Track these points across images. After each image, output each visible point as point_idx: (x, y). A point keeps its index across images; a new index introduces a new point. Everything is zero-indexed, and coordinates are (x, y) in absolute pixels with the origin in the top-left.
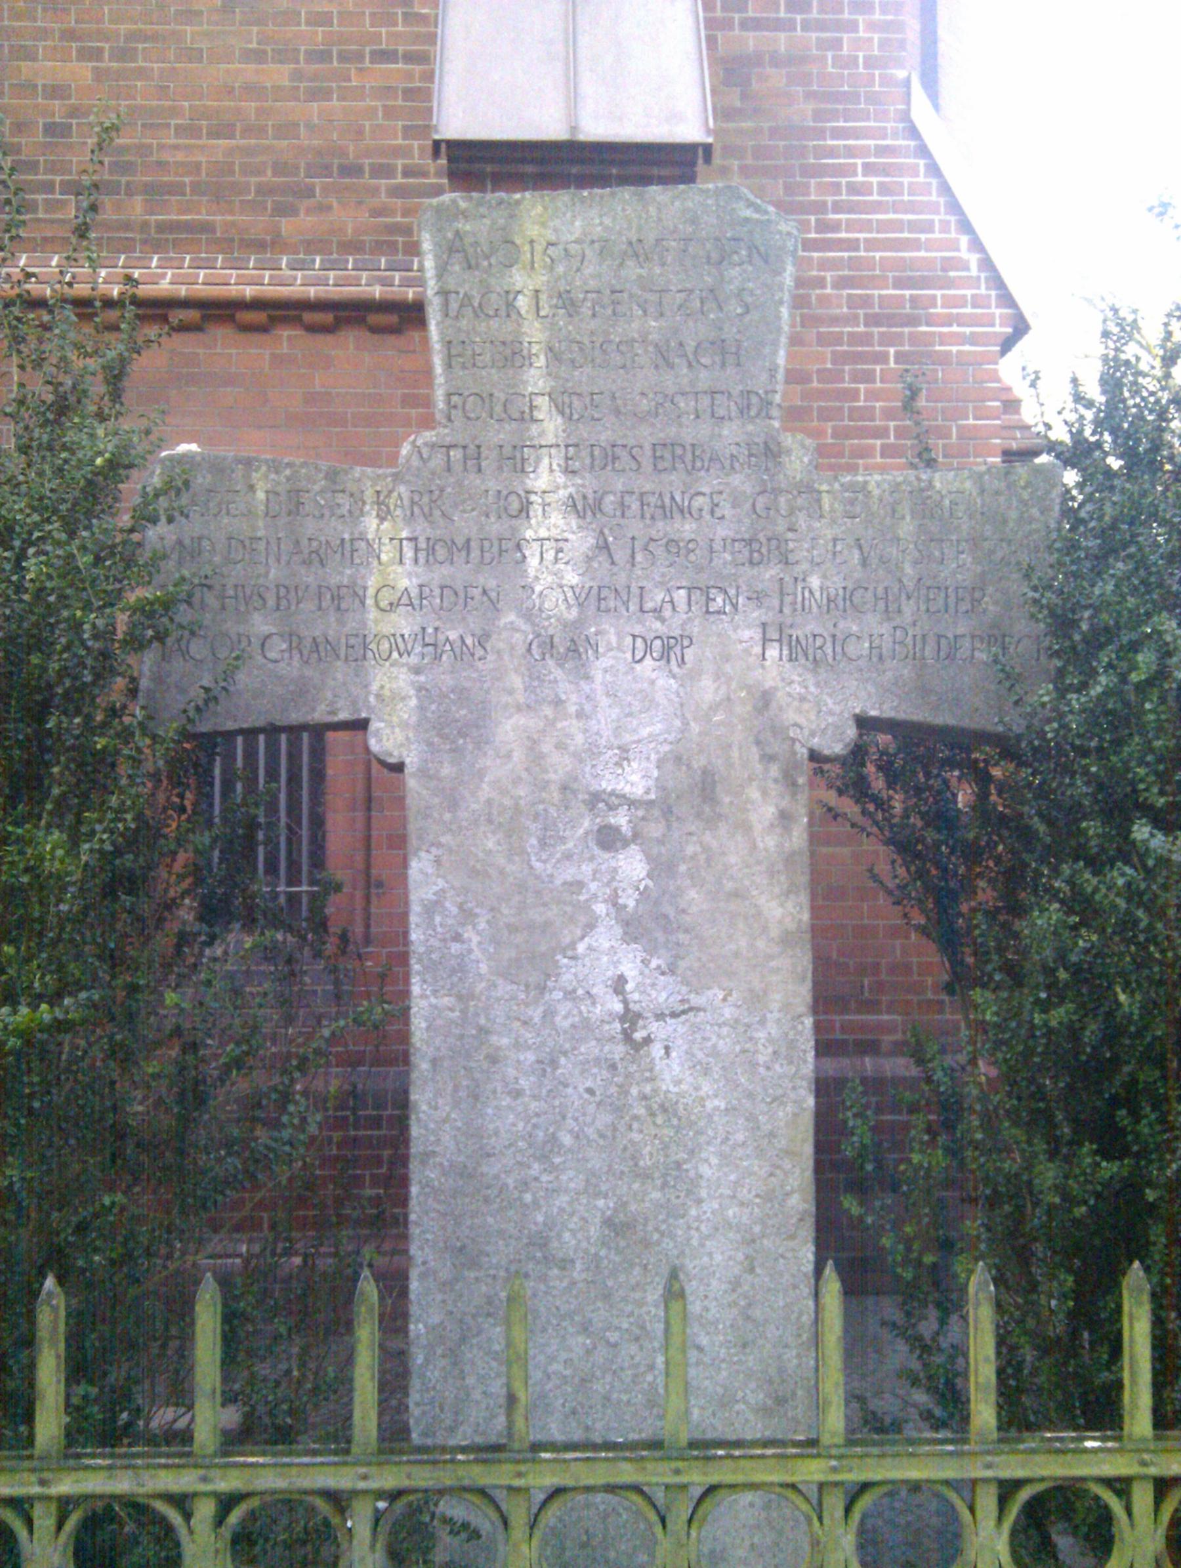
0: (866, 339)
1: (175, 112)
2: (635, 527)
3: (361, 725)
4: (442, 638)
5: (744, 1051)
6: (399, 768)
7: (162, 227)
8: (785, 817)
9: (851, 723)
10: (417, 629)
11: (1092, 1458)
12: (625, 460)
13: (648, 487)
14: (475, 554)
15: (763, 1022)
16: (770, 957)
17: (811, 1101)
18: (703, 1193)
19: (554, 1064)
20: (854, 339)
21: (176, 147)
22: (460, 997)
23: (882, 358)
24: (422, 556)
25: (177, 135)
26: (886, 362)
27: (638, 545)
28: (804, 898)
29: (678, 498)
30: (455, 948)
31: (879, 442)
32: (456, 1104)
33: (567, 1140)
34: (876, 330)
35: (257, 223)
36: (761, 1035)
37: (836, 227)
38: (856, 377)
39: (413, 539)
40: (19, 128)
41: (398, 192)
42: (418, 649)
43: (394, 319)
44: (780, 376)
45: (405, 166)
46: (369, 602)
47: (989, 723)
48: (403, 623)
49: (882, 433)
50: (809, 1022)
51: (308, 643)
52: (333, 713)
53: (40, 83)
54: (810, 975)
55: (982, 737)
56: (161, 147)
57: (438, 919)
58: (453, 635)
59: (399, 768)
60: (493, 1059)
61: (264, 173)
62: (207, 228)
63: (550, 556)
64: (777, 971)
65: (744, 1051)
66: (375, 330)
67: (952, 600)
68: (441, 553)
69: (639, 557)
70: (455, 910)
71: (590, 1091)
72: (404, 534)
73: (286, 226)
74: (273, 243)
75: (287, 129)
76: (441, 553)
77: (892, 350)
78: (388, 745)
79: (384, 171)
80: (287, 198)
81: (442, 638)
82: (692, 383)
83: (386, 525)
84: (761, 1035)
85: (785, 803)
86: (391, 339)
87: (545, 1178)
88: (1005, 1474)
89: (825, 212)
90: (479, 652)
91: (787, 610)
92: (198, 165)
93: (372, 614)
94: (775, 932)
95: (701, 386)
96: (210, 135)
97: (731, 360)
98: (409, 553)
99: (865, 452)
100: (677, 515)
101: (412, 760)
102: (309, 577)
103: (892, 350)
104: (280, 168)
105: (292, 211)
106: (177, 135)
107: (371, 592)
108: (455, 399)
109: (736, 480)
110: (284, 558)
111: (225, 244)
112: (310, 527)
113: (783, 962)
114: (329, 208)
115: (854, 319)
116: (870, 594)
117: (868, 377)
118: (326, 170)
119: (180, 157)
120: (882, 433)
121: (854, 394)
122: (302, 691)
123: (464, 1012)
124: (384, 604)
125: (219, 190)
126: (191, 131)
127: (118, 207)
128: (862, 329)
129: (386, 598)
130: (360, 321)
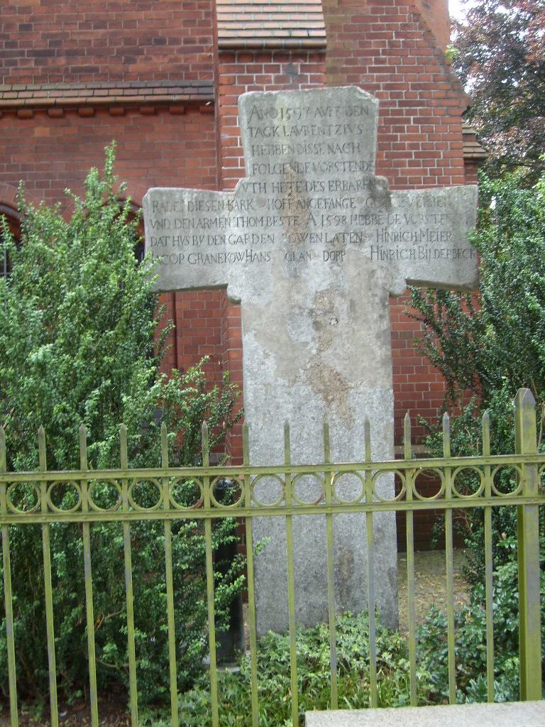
0: (400, 112)
1: (78, 17)
2: (324, 212)
3: (224, 287)
4: (253, 253)
5: (368, 403)
6: (239, 302)
7: (74, 70)
8: (381, 317)
9: (404, 282)
10: (244, 250)
11: (472, 461)
12: (319, 187)
13: (327, 197)
14: (265, 223)
15: (374, 392)
16: (378, 369)
17: (393, 420)
18: (355, 454)
19: (300, 408)
20: (395, 112)
21: (79, 34)
22: (265, 385)
23: (408, 121)
24: (245, 224)
25: (80, 28)
26: (410, 123)
27: (325, 218)
28: (389, 347)
29: (338, 200)
30: (263, 367)
31: (407, 160)
32: (265, 423)
33: (305, 436)
34: (404, 108)
35: (118, 68)
36: (374, 397)
37: (383, 62)
38: (396, 130)
39: (242, 218)
40: (9, 26)
41: (181, 51)
42: (245, 258)
43: (182, 109)
44: (374, 156)
45: (185, 39)
46: (227, 241)
47: (453, 281)
48: (240, 249)
49: (409, 155)
50: (391, 391)
51: (204, 257)
52: (214, 282)
53: (17, 6)
54: (391, 375)
55: (451, 287)
56: (72, 33)
57: (256, 357)
58: (258, 252)
59: (239, 302)
60: (278, 407)
61: (120, 44)
62: (95, 70)
63: (292, 223)
64: (379, 373)
65: (368, 403)
66: (173, 113)
67: (439, 237)
68: (252, 222)
69: (325, 222)
70: (262, 353)
71: (313, 418)
72: (239, 216)
73: (131, 68)
74: (125, 76)
75: (130, 24)
76: (252, 222)
77: (412, 117)
78: (236, 294)
79: (175, 41)
80: (130, 55)
81: (253, 253)
82: (342, 158)
83: (232, 213)
84: (374, 397)
85: (381, 312)
86: (180, 118)
87: (297, 449)
88: (453, 465)
89: (379, 55)
90: (267, 258)
91: (380, 241)
92: (89, 42)
93: (228, 245)
94: (378, 359)
95: (347, 160)
96: (95, 28)
97: (356, 150)
98: (240, 223)
99: (402, 164)
100: (339, 207)
101: (244, 300)
102: (206, 232)
103: (412, 117)
104: (128, 41)
105: (134, 61)
106: (80, 28)
107: (227, 237)
108: (256, 167)
109: (359, 194)
110: (196, 226)
111: (104, 76)
112: (205, 214)
113: (382, 371)
114: (151, 59)
115: (393, 104)
116: (410, 234)
117: (402, 130)
118: (148, 41)
119: (82, 37)
120: (409, 155)
121: (395, 138)
122: (202, 275)
123: (266, 390)
124: (232, 242)
125: (99, 51)
126: (86, 25)
127: (54, 62)
128: (397, 108)
129: (233, 239)
130: (167, 110)
